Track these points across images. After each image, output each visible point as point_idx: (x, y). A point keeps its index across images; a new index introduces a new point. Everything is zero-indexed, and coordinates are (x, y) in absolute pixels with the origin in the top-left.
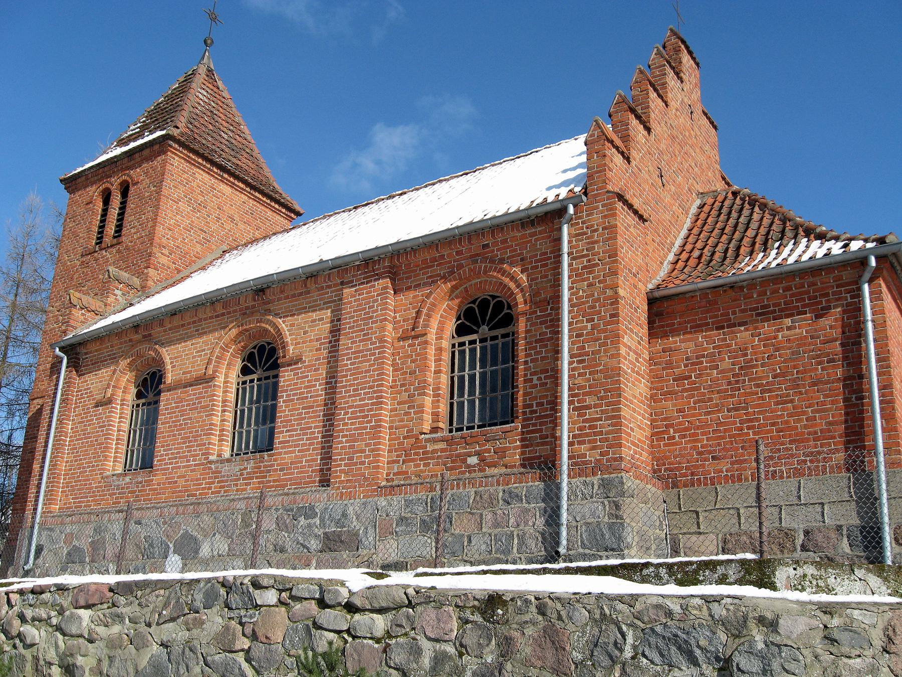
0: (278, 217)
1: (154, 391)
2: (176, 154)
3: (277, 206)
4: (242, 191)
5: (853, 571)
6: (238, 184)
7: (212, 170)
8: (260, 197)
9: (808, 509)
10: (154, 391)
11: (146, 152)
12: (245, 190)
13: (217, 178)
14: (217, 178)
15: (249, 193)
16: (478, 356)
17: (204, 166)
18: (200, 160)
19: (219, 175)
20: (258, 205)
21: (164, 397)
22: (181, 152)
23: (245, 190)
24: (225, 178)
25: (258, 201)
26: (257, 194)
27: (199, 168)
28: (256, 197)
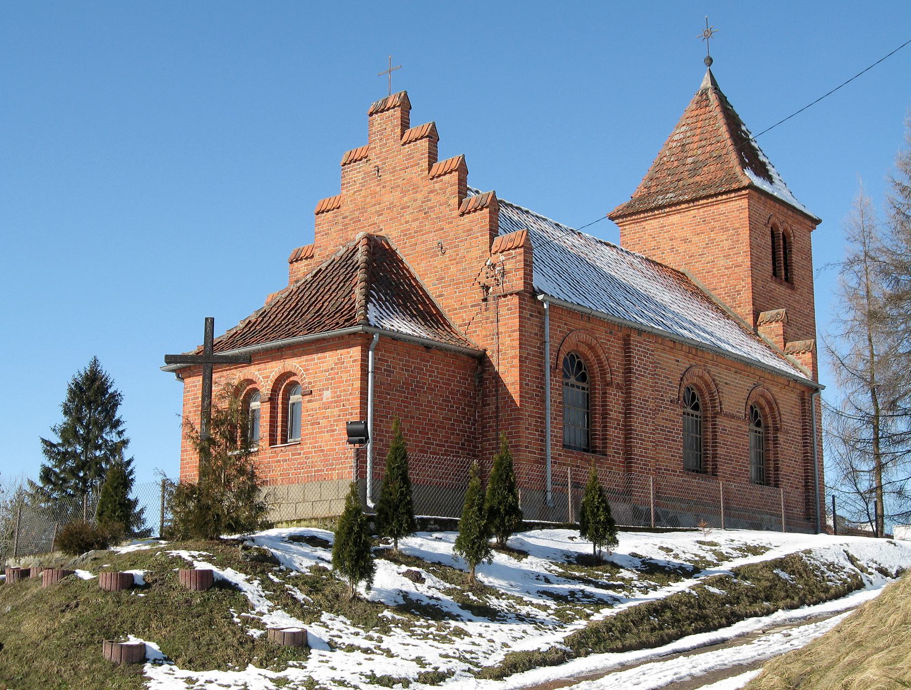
0: (731, 204)
1: (573, 367)
2: (625, 225)
3: (724, 197)
4: (688, 209)
5: (716, 475)
6: (680, 207)
7: (655, 215)
8: (705, 201)
9: (612, 252)
10: (573, 367)
11: (182, 360)
12: (690, 207)
13: (664, 216)
14: (664, 216)
15: (695, 206)
16: (280, 397)
17: (648, 216)
18: (642, 215)
19: (662, 213)
20: (709, 208)
21: (340, 509)
22: (626, 221)
23: (690, 207)
24: (669, 212)
25: (703, 206)
26: (701, 202)
27: (647, 220)
28: (703, 204)
